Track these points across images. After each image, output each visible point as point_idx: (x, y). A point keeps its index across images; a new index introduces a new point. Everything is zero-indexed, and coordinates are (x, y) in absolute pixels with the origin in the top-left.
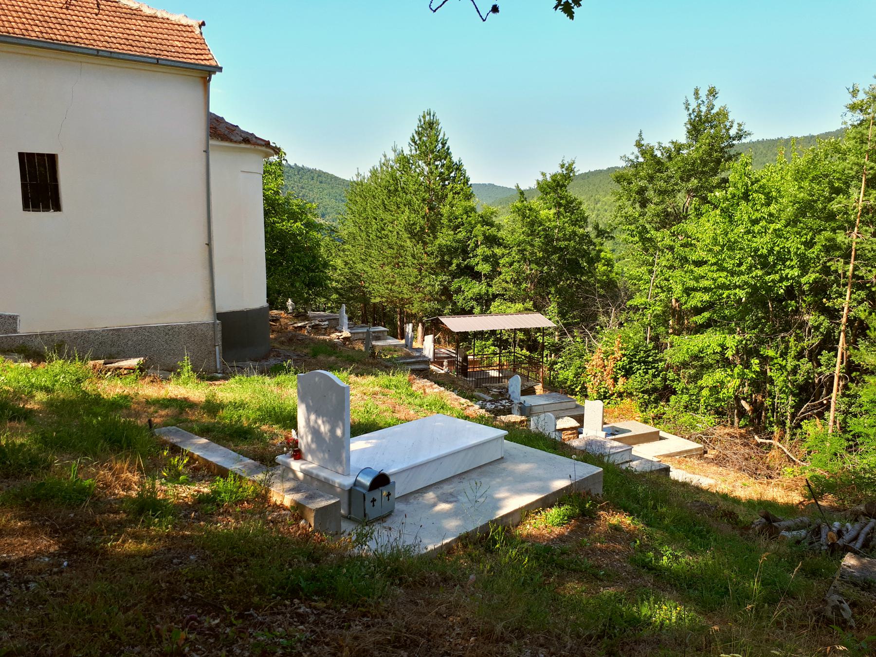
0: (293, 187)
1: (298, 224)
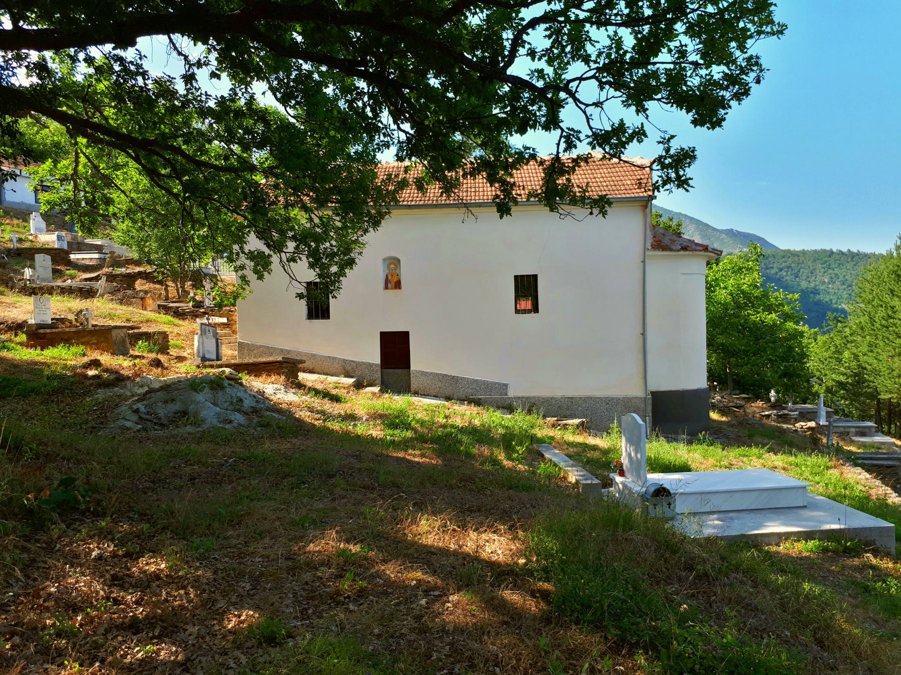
0: (845, 276)
1: (774, 315)
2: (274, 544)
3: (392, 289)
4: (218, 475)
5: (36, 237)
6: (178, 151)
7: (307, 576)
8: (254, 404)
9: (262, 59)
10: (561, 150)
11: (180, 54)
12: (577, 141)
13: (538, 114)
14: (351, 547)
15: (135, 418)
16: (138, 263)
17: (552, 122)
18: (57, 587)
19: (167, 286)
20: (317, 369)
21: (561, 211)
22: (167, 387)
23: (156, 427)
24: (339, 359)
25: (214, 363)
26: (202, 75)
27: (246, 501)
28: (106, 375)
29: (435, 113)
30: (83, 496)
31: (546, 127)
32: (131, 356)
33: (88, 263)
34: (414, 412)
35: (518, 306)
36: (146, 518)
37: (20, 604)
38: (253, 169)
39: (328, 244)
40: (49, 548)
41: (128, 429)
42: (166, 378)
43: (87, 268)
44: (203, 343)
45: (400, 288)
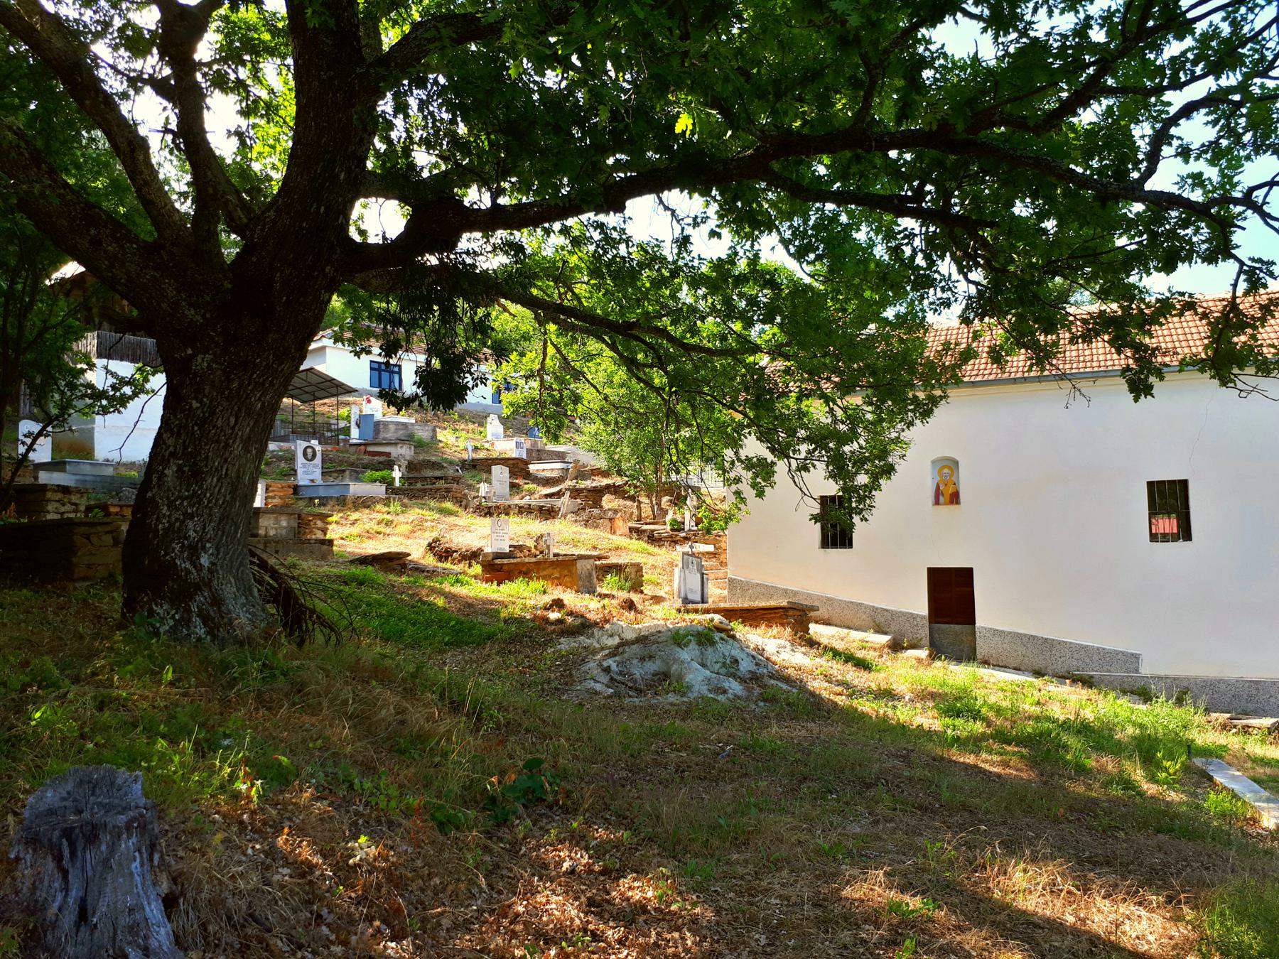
2: (796, 881)
3: (945, 504)
4: (714, 768)
5: (493, 444)
6: (663, 333)
7: (845, 936)
8: (753, 668)
9: (773, 204)
10: (1240, 292)
11: (667, 208)
12: (1267, 277)
13: (1195, 239)
14: (907, 898)
15: (604, 679)
16: (605, 474)
17: (1221, 249)
18: (526, 907)
19: (640, 502)
20: (834, 620)
21: (1240, 385)
22: (642, 640)
23: (631, 693)
24: (866, 607)
25: (700, 606)
26: (699, 238)
27: (754, 811)
28: (570, 619)
29: (1026, 253)
30: (550, 785)
31: (1210, 258)
32: (600, 595)
33: (548, 474)
34: (983, 692)
35: (1153, 527)
36: (624, 821)
37: (484, 923)
38: (756, 349)
39: (855, 445)
40: (513, 851)
41: (597, 693)
42: (640, 626)
43: (548, 482)
44: (685, 579)
45: (958, 502)
